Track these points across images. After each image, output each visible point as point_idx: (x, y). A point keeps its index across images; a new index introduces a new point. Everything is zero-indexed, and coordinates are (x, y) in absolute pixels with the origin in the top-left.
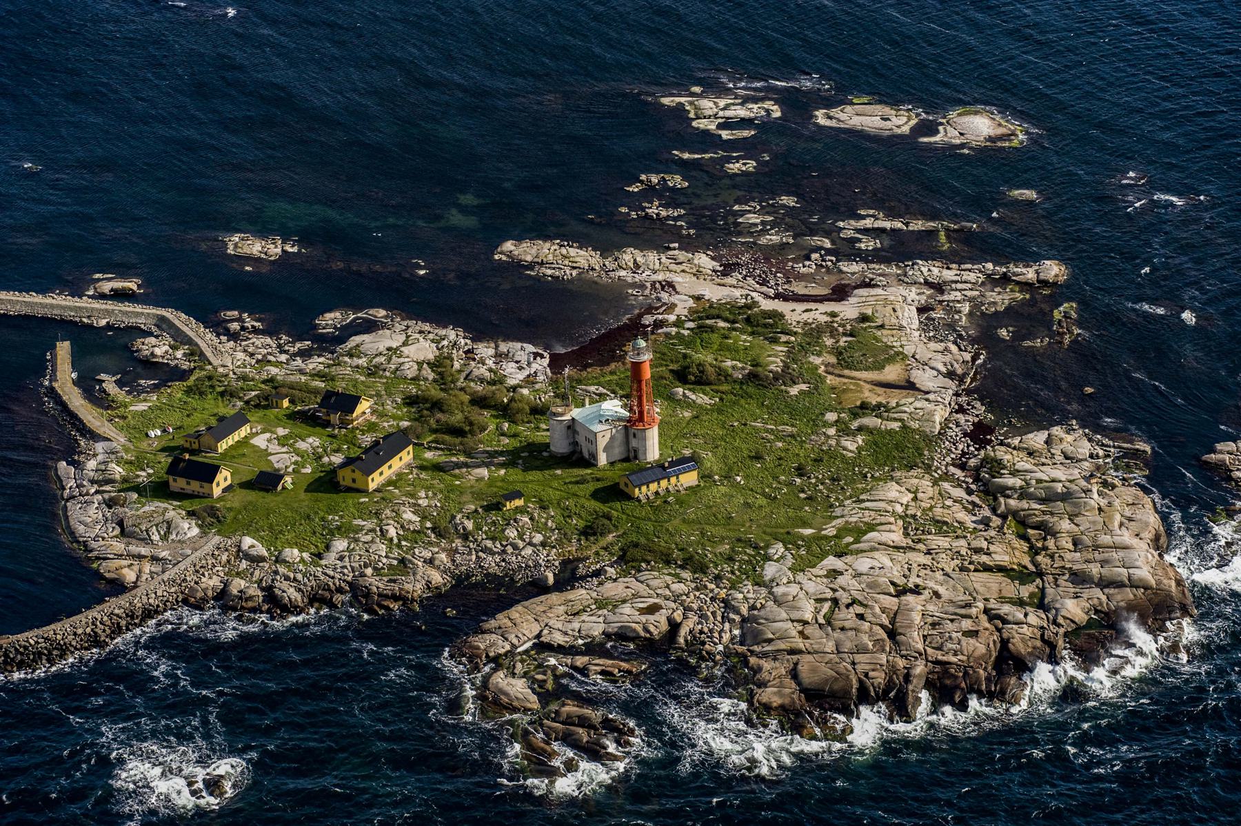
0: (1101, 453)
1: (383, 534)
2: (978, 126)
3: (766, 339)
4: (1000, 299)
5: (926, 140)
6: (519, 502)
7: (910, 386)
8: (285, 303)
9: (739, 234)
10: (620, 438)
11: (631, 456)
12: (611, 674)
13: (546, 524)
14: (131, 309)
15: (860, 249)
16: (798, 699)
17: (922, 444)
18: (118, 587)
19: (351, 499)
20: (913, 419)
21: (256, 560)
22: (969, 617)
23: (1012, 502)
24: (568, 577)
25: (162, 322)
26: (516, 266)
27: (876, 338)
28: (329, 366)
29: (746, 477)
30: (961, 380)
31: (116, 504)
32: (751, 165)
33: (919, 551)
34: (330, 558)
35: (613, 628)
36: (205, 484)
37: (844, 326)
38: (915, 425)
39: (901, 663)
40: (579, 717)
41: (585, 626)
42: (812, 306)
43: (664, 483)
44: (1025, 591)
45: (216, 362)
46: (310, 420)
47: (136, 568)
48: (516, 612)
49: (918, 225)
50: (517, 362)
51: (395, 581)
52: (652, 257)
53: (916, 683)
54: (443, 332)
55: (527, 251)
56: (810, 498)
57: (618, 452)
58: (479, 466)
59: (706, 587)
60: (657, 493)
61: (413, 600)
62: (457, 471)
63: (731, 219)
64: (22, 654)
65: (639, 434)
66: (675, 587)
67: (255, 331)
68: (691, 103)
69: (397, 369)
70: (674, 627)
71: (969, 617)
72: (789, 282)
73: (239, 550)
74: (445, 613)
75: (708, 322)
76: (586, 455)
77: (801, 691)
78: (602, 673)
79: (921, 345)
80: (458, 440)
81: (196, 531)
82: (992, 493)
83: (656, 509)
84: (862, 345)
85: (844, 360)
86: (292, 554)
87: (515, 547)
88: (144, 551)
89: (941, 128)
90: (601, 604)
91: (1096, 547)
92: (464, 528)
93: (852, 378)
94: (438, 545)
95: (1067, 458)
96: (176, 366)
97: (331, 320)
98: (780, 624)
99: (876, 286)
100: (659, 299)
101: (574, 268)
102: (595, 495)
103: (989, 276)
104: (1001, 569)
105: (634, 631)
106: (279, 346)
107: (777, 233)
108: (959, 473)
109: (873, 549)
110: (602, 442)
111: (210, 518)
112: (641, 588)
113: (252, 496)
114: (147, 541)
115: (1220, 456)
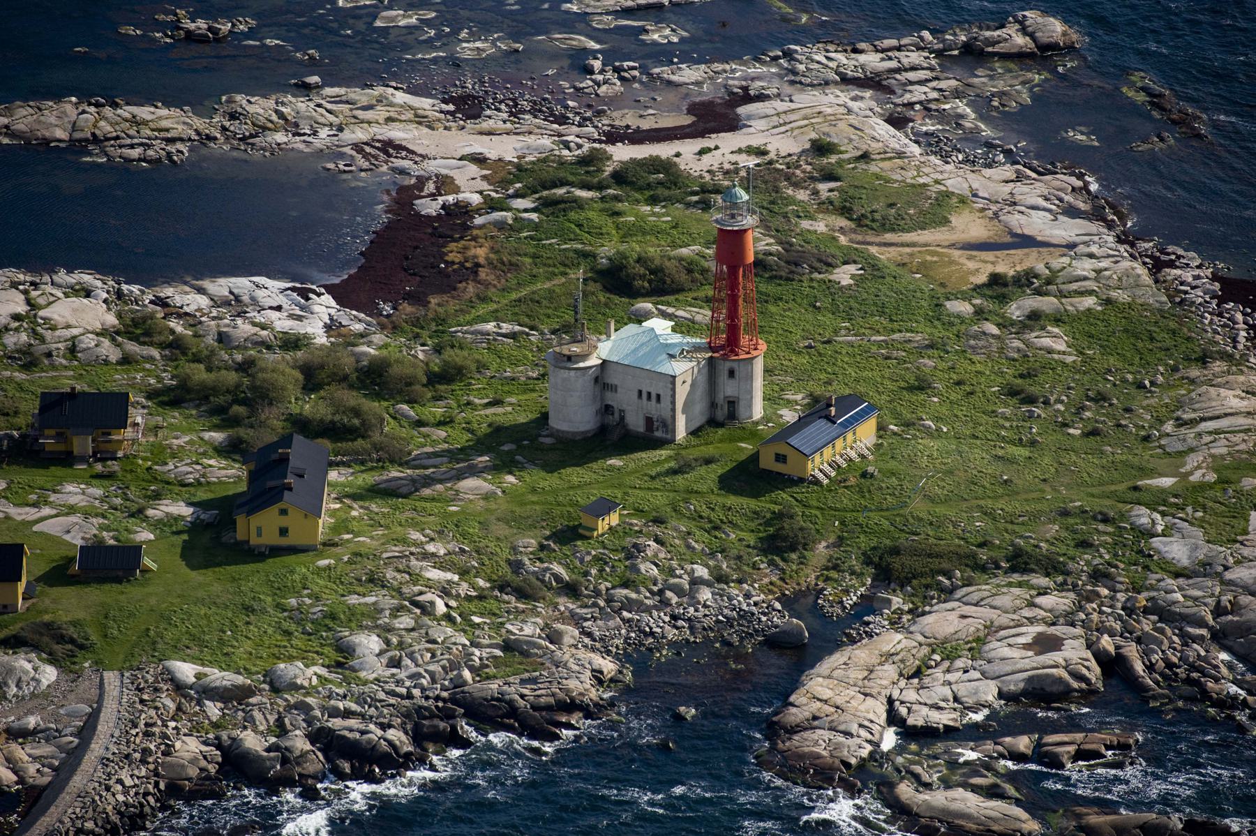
3: (689, 205)
6: (614, 519)
7: (1026, 242)
9: (406, 48)
10: (703, 380)
11: (721, 415)
12: (1097, 755)
13: (689, 547)
19: (300, 567)
20: (1109, 287)
21: (234, 696)
27: (878, 177)
35: (1015, 684)
41: (962, 690)
43: (839, 443)
54: (1029, 75)
62: (427, 492)
63: (361, 26)
65: (740, 371)
70: (1113, 665)
72: (600, 113)
73: (179, 687)
75: (561, 191)
76: (636, 423)
78: (1080, 755)
79: (970, 176)
81: (50, 674)
87: (679, 591)
92: (557, 578)
93: (903, 245)
105: (1060, 680)
112: (986, 613)
113: (96, 595)
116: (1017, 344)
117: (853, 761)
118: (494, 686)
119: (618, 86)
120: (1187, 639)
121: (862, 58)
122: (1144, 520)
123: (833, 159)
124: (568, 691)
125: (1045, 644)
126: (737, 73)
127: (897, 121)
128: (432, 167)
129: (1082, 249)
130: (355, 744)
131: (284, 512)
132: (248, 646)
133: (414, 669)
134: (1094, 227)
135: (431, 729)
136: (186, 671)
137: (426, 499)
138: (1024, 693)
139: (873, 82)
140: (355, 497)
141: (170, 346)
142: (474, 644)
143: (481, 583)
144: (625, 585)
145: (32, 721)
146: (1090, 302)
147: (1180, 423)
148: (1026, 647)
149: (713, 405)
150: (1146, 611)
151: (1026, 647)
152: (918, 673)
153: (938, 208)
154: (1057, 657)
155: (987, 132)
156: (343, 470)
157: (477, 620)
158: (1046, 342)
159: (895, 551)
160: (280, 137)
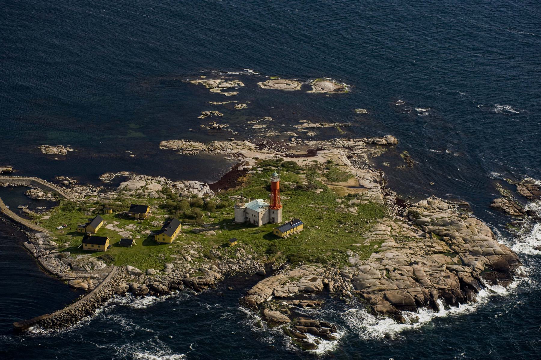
0: (452, 207)
1: (186, 260)
2: (328, 86)
3: (294, 172)
4: (377, 151)
5: (309, 92)
6: (236, 243)
7: (362, 187)
8: (86, 173)
9: (256, 133)
10: (267, 214)
11: (271, 221)
12: (311, 306)
13: (250, 250)
14: (17, 178)
15: (309, 136)
16: (394, 308)
17: (381, 208)
18: (82, 291)
19: (165, 247)
20: (372, 199)
21: (138, 275)
22: (443, 271)
23: (431, 227)
24: (271, 272)
25: (33, 183)
26: (171, 151)
27: (338, 169)
28: (119, 196)
29: (320, 226)
30: (380, 182)
31: (63, 257)
32: (244, 106)
33: (406, 248)
34: (169, 271)
35: (302, 288)
36: (101, 246)
37: (322, 166)
38: (374, 201)
39: (427, 290)
40: (310, 323)
41: (291, 289)
42: (306, 159)
43: (292, 230)
44: (455, 260)
45: (68, 198)
46: (126, 217)
47: (86, 282)
48: (260, 285)
49: (326, 125)
50: (197, 189)
51: (201, 278)
52: (227, 144)
53: (436, 297)
55: (175, 144)
56: (350, 232)
57: (266, 221)
58: (209, 230)
59: (330, 269)
60: (290, 235)
61: (212, 285)
62: (201, 233)
63: (250, 127)
64: (59, 321)
65: (275, 212)
66: (318, 270)
67: (75, 184)
68: (205, 82)
69: (149, 195)
70: (326, 286)
71: (443, 271)
72: (288, 150)
73: (128, 271)
74: (229, 289)
75: (268, 167)
76: (252, 222)
77: (392, 305)
78: (308, 306)
79: (357, 171)
80: (194, 221)
81: (104, 265)
82: (420, 225)
83: (293, 241)
84: (332, 172)
85: (330, 178)
86: (152, 271)
87: (243, 260)
88: (86, 275)
89: (313, 87)
90: (292, 279)
91: (474, 241)
92: (218, 255)
94: (210, 262)
95: (440, 209)
96: (50, 200)
97: (106, 177)
98: (370, 280)
99: (324, 149)
100: (240, 160)
101: (197, 150)
102: (265, 237)
103: (367, 143)
104: (441, 252)
105: (312, 288)
106: (90, 189)
107: (272, 131)
108: (402, 218)
109: (388, 249)
110: (261, 216)
111: (108, 259)
112: (305, 272)
113: (121, 249)
114: (85, 271)
115: (498, 204)
116: (346, 210)
117: (259, 303)
118: (192, 278)
119: (295, 145)
120: (345, 281)
121: (349, 142)
122: (349, 253)
123: (331, 164)
124: (206, 281)
125: (314, 279)
126: (321, 143)
127: (349, 157)
128: (246, 159)
129: (372, 190)
130: (155, 288)
131: (164, 235)
132: (146, 264)
133: (177, 273)
134: (378, 185)
135: (173, 287)
136: (130, 268)
137: (202, 235)
138: (304, 290)
139: (350, 148)
140: (185, 233)
141: (169, 195)
142: (192, 268)
143: (202, 255)
144: (232, 258)
145: (96, 276)
146: (367, 202)
147: (370, 231)
148: (309, 280)
149: (270, 219)
150: (340, 274)
151: (309, 280)
152: (283, 284)
153: (347, 177)
154: (314, 283)
155: (367, 161)
156: (188, 226)
157: (196, 263)
158: (352, 210)
159: (293, 256)
160: (219, 151)
